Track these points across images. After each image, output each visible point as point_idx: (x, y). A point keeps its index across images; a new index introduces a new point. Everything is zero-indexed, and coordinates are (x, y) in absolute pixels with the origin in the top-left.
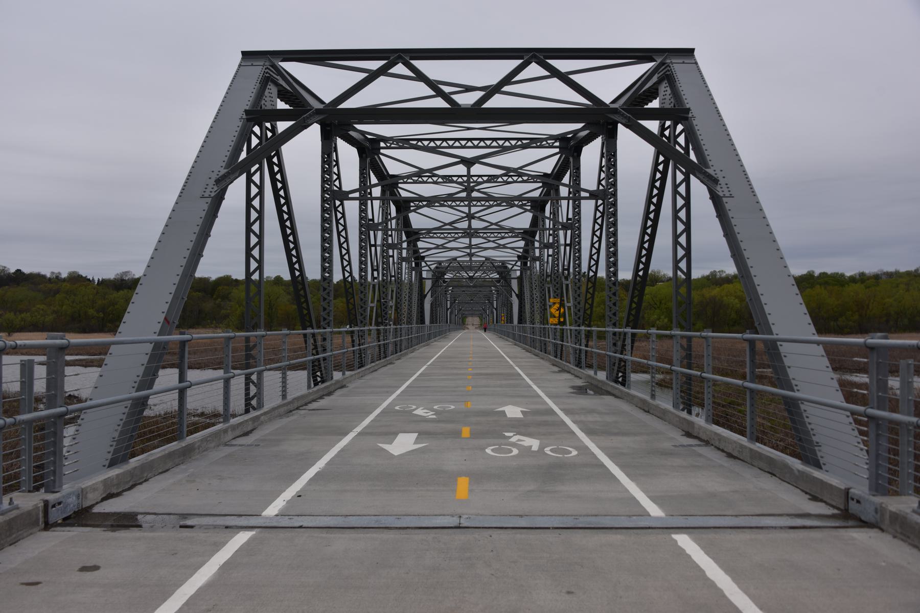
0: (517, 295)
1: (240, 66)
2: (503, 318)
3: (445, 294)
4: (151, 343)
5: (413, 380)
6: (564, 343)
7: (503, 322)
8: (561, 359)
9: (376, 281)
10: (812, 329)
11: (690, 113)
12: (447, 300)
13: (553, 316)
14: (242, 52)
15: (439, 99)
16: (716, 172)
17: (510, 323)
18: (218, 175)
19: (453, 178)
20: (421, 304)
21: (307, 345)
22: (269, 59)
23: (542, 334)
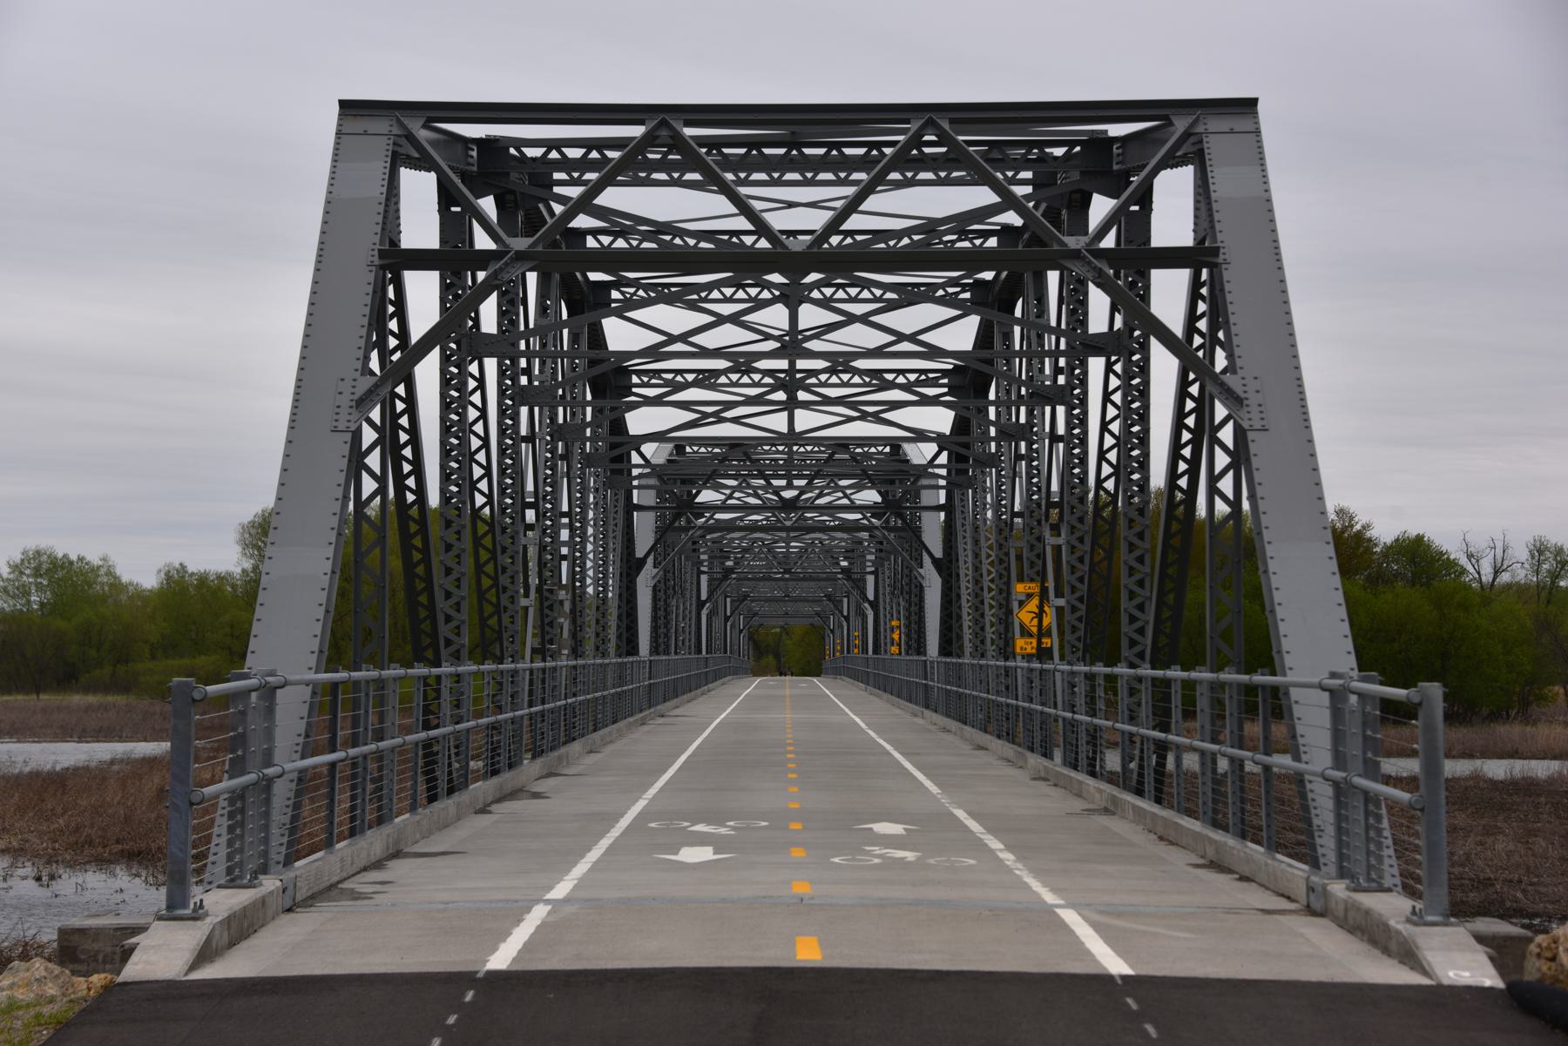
0: (935, 561)
1: (339, 133)
2: (896, 636)
3: (694, 550)
4: (308, 685)
5: (622, 815)
6: (1171, 737)
7: (895, 649)
8: (1158, 801)
9: (530, 533)
10: (1352, 661)
11: (1221, 255)
12: (700, 573)
13: (1025, 632)
14: (346, 105)
15: (742, 218)
16: (1246, 389)
17: (919, 653)
18: (353, 394)
19: (742, 237)
20: (628, 588)
21: (534, 687)
22: (398, 120)
23: (1036, 693)
